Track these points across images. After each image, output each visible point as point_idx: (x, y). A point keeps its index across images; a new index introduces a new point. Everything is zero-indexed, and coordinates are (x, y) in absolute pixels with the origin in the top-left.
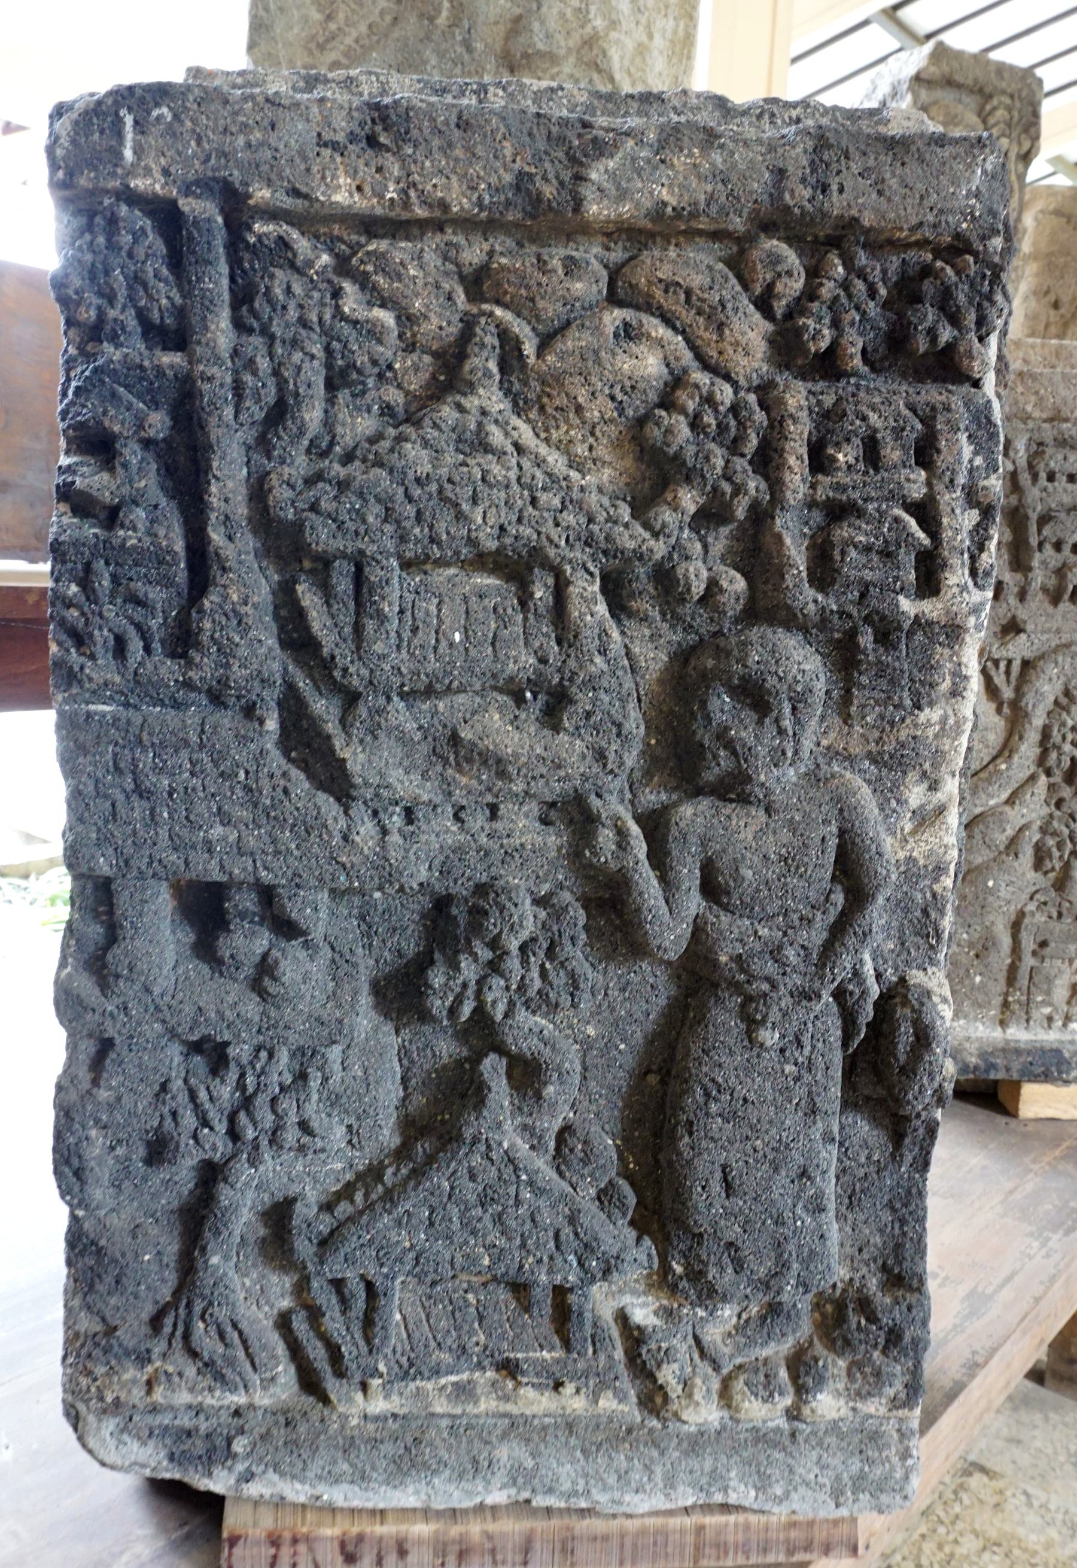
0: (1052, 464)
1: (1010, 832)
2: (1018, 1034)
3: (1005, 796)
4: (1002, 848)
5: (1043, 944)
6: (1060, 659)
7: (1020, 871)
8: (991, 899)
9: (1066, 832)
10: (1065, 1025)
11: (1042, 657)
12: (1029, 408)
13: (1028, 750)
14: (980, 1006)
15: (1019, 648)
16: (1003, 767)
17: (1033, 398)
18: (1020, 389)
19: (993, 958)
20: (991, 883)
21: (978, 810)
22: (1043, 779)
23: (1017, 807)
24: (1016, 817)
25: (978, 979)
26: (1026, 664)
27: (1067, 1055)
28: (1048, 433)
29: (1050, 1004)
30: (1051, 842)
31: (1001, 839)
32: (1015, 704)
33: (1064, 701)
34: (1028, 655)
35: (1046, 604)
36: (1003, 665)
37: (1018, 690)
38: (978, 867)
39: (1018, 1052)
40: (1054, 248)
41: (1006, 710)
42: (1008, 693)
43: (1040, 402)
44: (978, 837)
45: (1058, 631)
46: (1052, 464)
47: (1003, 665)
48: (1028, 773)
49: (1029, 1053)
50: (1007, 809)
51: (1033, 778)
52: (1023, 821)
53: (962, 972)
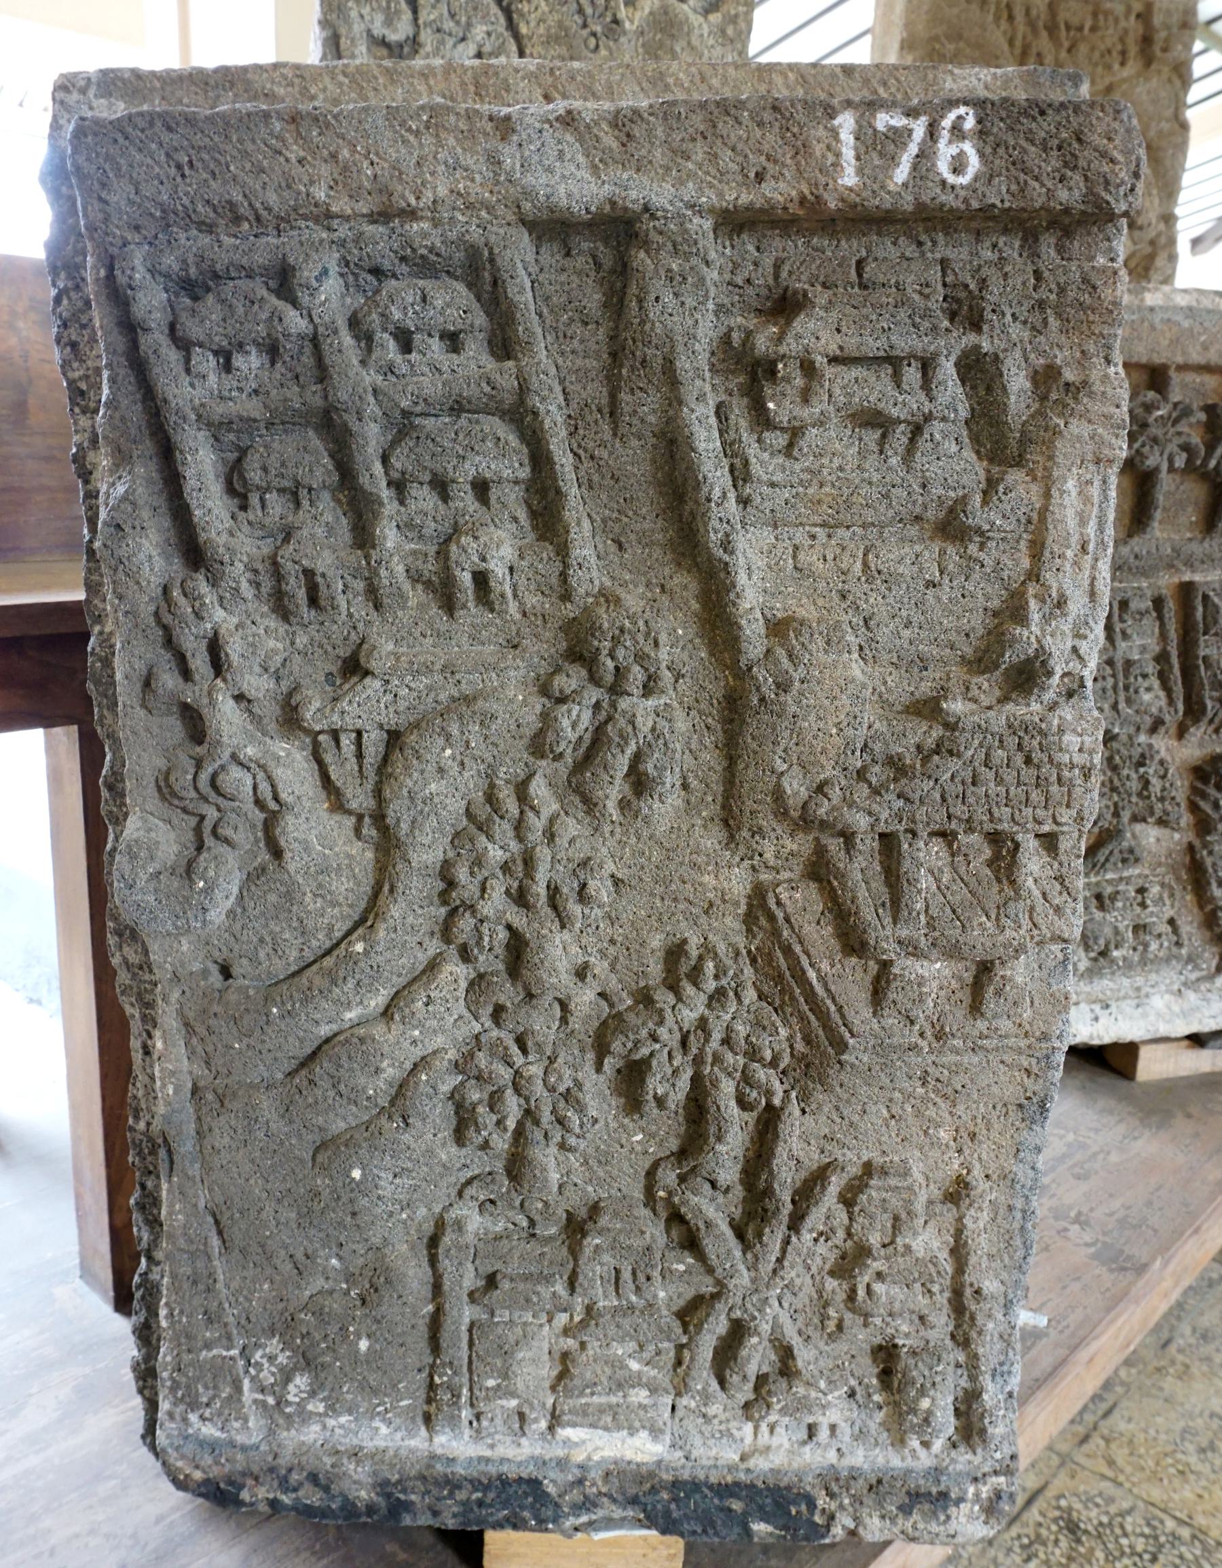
0: (397, 315)
1: (391, 1072)
2: (457, 1446)
3: (377, 1001)
4: (384, 1102)
5: (491, 1281)
6: (454, 729)
7: (419, 1147)
8: (364, 1202)
9: (506, 1074)
10: (551, 1428)
11: (416, 725)
12: (321, 194)
13: (411, 913)
14: (375, 1392)
15: (368, 708)
16: (359, 947)
17: (325, 170)
18: (295, 151)
19: (389, 1308)
20: (356, 1174)
21: (325, 1030)
22: (456, 972)
23: (396, 1028)
24: (398, 1047)
25: (364, 1345)
26: (394, 738)
27: (551, 1489)
28: (380, 242)
29: (513, 1395)
30: (474, 1095)
31: (378, 1087)
32: (379, 818)
33: (483, 812)
34: (392, 720)
35: (434, 610)
36: (347, 741)
37: (378, 793)
38: (333, 1139)
39: (452, 1484)
40: (939, 30)
41: (369, 830)
42: (359, 798)
43: (344, 176)
44: (325, 1083)
45: (449, 669)
46: (397, 315)
47: (347, 741)
48: (422, 958)
49: (476, 1484)
50: (378, 1030)
51: (433, 966)
52: (418, 1052)
53: (332, 1330)
